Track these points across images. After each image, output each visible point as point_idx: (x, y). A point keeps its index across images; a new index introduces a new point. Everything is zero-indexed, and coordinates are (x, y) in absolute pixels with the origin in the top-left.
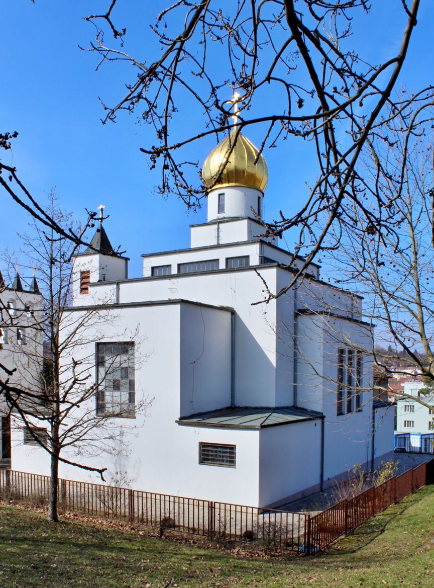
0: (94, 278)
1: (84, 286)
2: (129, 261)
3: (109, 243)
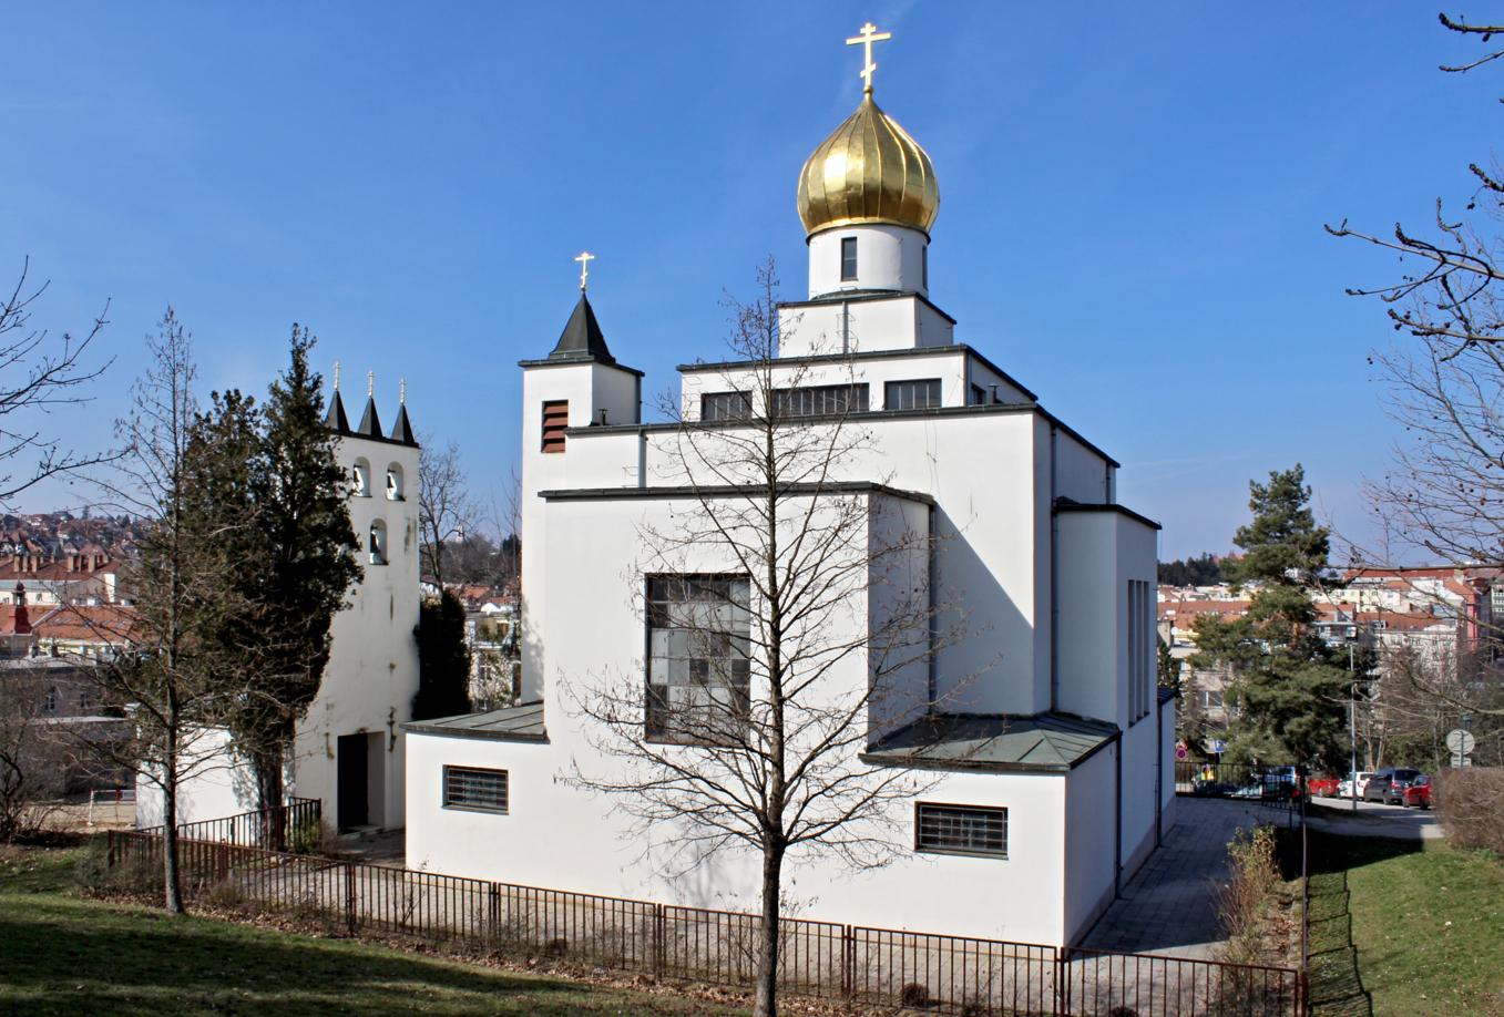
0: (580, 416)
1: (552, 435)
2: (642, 379)
3: (601, 337)
